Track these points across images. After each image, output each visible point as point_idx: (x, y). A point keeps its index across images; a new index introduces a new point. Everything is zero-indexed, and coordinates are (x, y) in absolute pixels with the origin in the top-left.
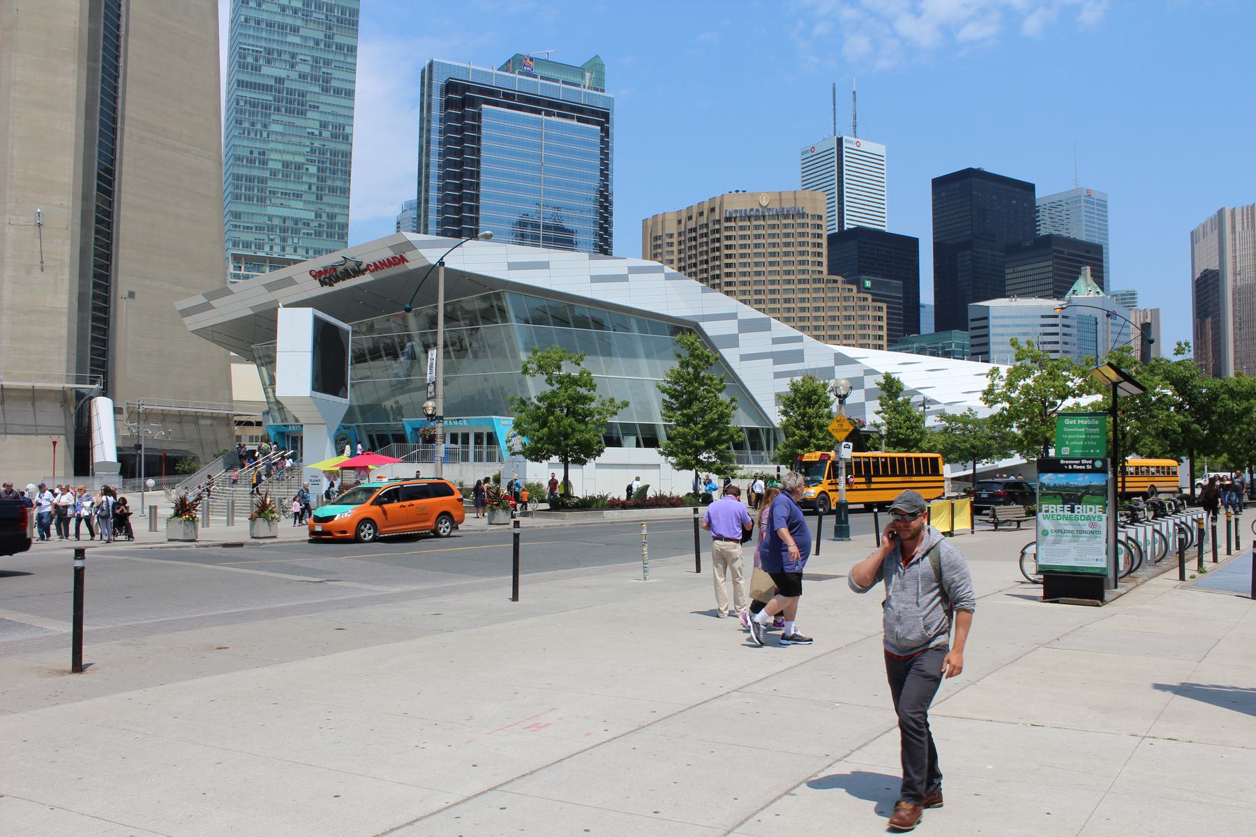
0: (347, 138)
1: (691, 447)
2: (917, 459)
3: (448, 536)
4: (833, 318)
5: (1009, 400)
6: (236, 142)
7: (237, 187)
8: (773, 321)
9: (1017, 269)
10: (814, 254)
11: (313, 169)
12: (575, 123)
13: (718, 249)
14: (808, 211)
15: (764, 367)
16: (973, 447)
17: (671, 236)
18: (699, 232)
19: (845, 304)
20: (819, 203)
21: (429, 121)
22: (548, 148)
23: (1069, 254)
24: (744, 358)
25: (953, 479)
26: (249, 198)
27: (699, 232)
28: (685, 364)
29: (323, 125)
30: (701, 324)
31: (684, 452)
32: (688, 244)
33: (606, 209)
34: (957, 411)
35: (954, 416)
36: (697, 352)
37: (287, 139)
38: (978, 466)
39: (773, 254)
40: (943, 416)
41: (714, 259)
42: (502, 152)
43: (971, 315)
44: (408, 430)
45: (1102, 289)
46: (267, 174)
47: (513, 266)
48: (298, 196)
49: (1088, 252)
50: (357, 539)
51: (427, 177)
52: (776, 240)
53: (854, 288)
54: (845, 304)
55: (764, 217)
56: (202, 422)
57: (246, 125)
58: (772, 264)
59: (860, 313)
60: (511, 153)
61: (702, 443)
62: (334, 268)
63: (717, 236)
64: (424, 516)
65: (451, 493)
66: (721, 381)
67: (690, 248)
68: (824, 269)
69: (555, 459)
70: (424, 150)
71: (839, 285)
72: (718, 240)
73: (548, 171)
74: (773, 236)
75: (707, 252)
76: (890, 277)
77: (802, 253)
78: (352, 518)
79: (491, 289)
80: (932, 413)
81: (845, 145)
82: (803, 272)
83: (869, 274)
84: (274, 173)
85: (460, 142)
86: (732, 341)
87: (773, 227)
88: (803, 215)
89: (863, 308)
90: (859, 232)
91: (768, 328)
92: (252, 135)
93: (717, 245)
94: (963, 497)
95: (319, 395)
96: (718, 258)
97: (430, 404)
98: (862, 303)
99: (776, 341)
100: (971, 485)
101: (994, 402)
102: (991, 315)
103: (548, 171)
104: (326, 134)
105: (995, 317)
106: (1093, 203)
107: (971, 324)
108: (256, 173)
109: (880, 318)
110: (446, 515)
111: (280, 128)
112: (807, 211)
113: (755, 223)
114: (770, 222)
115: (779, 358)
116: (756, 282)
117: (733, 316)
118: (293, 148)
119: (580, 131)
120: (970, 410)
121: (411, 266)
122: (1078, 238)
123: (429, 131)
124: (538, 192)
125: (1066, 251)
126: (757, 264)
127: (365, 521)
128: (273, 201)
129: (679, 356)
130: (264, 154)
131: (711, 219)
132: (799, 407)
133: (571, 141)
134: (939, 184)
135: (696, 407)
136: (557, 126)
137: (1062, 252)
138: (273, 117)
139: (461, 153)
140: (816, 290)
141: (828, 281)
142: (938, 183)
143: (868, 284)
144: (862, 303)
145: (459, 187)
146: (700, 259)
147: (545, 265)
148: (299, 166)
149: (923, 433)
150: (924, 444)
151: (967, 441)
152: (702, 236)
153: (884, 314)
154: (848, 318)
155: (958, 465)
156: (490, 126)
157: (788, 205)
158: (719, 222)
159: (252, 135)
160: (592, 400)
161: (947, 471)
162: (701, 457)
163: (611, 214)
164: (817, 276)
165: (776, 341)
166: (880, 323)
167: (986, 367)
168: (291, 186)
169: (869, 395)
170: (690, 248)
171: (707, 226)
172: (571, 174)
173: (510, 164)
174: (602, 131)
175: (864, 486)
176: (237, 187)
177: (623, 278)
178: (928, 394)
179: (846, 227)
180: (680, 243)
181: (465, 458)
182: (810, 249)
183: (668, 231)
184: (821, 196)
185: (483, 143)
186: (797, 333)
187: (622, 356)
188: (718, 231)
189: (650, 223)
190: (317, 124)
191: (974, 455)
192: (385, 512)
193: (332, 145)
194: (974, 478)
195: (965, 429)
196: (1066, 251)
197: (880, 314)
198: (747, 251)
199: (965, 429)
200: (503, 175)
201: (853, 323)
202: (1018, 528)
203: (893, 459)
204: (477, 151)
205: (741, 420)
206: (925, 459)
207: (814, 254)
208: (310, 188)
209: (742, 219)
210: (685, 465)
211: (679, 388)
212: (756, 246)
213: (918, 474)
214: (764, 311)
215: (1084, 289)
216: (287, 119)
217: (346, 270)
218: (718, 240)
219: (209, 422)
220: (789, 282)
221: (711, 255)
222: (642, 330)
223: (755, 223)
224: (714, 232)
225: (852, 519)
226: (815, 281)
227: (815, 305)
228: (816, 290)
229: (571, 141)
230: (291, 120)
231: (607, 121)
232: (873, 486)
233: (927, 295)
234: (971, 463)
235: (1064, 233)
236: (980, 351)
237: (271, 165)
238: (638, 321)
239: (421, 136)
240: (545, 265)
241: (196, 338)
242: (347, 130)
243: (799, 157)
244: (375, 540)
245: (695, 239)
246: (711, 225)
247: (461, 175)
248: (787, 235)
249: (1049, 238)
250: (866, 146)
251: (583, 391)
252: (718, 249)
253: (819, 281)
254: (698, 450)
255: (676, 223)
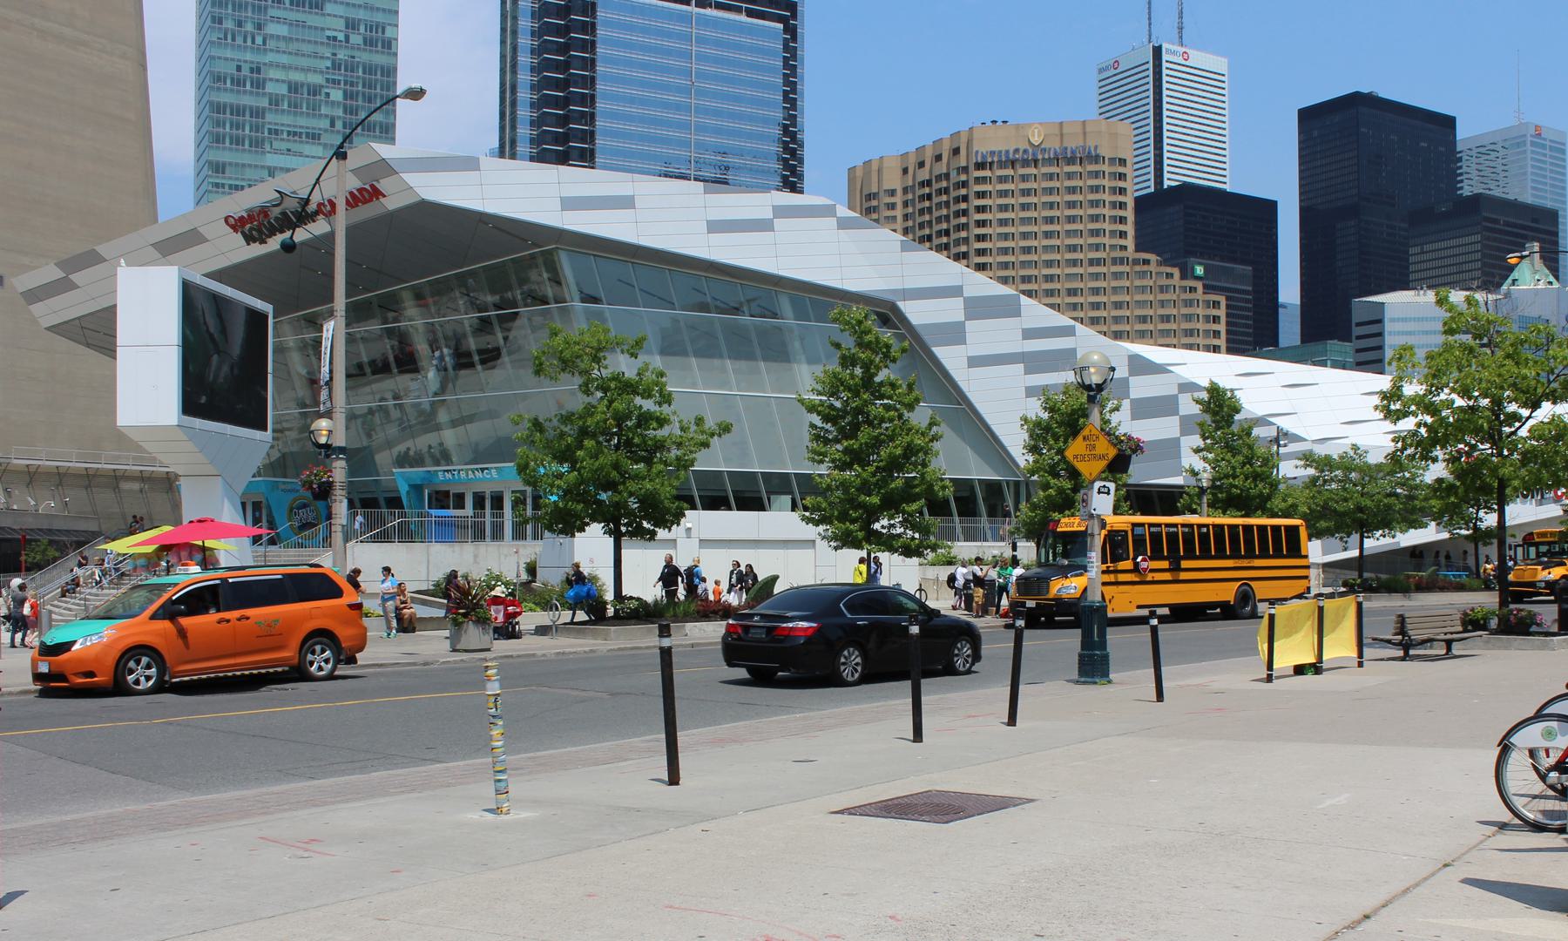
0: (389, 45)
1: (855, 509)
2: (1262, 528)
3: (331, 677)
4: (1143, 319)
5: (1431, 409)
6: (215, 52)
7: (218, 123)
8: (1024, 299)
9: (1426, 247)
10: (1114, 219)
11: (337, 95)
12: (743, 18)
13: (965, 213)
14: (1105, 152)
15: (999, 365)
16: (1360, 509)
17: (892, 193)
18: (935, 186)
19: (1161, 297)
20: (1122, 139)
21: (515, 18)
22: (701, 58)
23: (1507, 224)
24: (975, 362)
25: (1326, 566)
26: (238, 141)
27: (935, 186)
28: (848, 361)
29: (351, 25)
30: (901, 304)
31: (843, 517)
32: (919, 206)
33: (793, 153)
34: (1334, 451)
35: (1328, 457)
36: (868, 338)
37: (293, 47)
38: (1368, 543)
39: (1049, 220)
40: (1308, 458)
41: (959, 228)
42: (630, 63)
43: (1356, 317)
44: (403, 489)
45: (1557, 278)
46: (264, 103)
47: (569, 204)
48: (314, 137)
49: (1535, 221)
50: (118, 688)
51: (514, 103)
52: (1054, 198)
53: (1176, 272)
54: (1161, 297)
55: (1036, 161)
56: (125, 486)
57: (229, 24)
58: (1048, 235)
59: (1185, 311)
60: (645, 66)
61: (875, 500)
62: (264, 211)
63: (963, 192)
64: (272, 637)
65: (337, 592)
66: (910, 387)
67: (922, 212)
68: (1130, 242)
69: (596, 529)
70: (508, 65)
71: (1153, 267)
72: (965, 198)
73: (701, 93)
74: (1050, 191)
75: (947, 218)
76: (1234, 260)
77: (1095, 218)
78: (108, 646)
79: (536, 245)
80: (1290, 456)
81: (1165, 57)
82: (1097, 247)
83: (1202, 256)
84: (275, 101)
85: (563, 49)
86: (955, 334)
87: (1051, 177)
88: (1096, 159)
89: (1188, 303)
90: (1185, 189)
91: (1016, 312)
92: (239, 40)
93: (963, 206)
94: (1342, 595)
95: (198, 423)
96: (965, 227)
97: (323, 423)
98: (1188, 296)
99: (1029, 334)
100: (1355, 574)
101: (1404, 414)
102: (1388, 315)
103: (701, 93)
104: (356, 39)
105: (1393, 320)
106: (1544, 147)
107: (1357, 331)
108: (247, 101)
109: (1216, 319)
110: (324, 636)
111: (282, 30)
112: (1103, 152)
113: (1022, 171)
114: (1045, 170)
115: (1033, 362)
116: (1024, 264)
117: (956, 291)
118: (304, 62)
119: (750, 30)
120: (1355, 448)
121: (392, 203)
122: (1521, 199)
123: (514, 33)
124: (685, 126)
125: (1502, 219)
126: (1025, 236)
127: (135, 651)
128: (276, 145)
129: (837, 346)
130: (259, 71)
131: (954, 165)
132: (1056, 440)
133: (738, 47)
134: (1308, 116)
135: (865, 435)
136: (715, 23)
137: (1496, 221)
138: (272, 12)
139: (566, 66)
140: (1117, 276)
141: (1136, 262)
142: (1308, 116)
143: (1199, 270)
144: (1188, 296)
145: (564, 121)
146: (936, 228)
147: (627, 202)
148: (314, 90)
149: (1274, 485)
150: (1276, 503)
151: (1351, 499)
152: (939, 192)
153: (1222, 312)
154: (1166, 319)
155: (1334, 541)
156: (608, 24)
157: (1072, 143)
158: (965, 170)
159: (239, 40)
160: (662, 422)
161: (1316, 551)
162: (877, 526)
163: (801, 161)
164: (1118, 254)
165: (1029, 334)
166: (1215, 327)
167: (1384, 382)
168: (302, 121)
169: (1187, 426)
170: (922, 212)
171: (947, 176)
172: (737, 99)
173: (643, 84)
174: (786, 31)
175: (1167, 576)
176: (218, 123)
177: (763, 226)
178: (1285, 424)
179: (1167, 184)
180: (906, 204)
181: (498, 534)
182: (1107, 212)
183: (887, 186)
184: (1125, 129)
185: (600, 50)
186: (1063, 320)
187: (765, 359)
188: (965, 184)
189: (859, 173)
190: (341, 24)
191: (1363, 522)
192: (182, 633)
193: (364, 57)
194: (1361, 563)
195: (1347, 479)
196: (1502, 219)
197: (1215, 312)
198: (1009, 215)
199: (1347, 479)
200: (632, 100)
201: (1173, 326)
202: (1449, 655)
203: (1219, 528)
204: (591, 64)
205: (954, 462)
206: (1276, 529)
207: (1114, 219)
208: (333, 124)
209: (1002, 165)
210: (846, 541)
211: (838, 404)
212: (1024, 207)
213: (1264, 554)
214: (1004, 281)
215: (1529, 276)
216: (293, 16)
217: (284, 213)
218: (965, 198)
219: (136, 486)
220: (1074, 263)
221: (954, 222)
222: (800, 314)
223: (1022, 171)
224: (959, 185)
225: (1114, 636)
226: (1115, 261)
227: (1115, 298)
228: (1117, 276)
229: (738, 47)
230: (300, 17)
231: (794, 16)
232: (1183, 576)
233: (1289, 290)
234: (1355, 537)
235: (1497, 192)
236: (1370, 361)
237: (270, 88)
238: (794, 302)
239: (503, 42)
240: (627, 202)
241: (63, 344)
242: (389, 33)
243: (1096, 77)
244: (160, 688)
245: (929, 197)
246: (953, 174)
247: (566, 102)
248: (1072, 190)
249: (1476, 199)
250: (1198, 58)
251: (648, 405)
252: (965, 213)
253: (1121, 261)
254: (873, 514)
255: (900, 172)
